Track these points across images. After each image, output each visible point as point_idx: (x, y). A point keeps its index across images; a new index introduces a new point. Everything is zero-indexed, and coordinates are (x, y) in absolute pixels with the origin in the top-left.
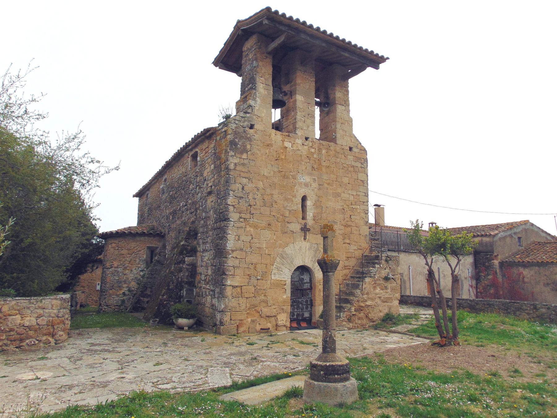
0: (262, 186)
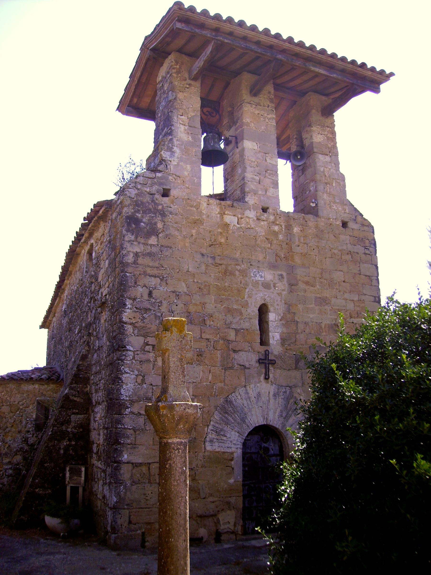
0: (185, 290)
